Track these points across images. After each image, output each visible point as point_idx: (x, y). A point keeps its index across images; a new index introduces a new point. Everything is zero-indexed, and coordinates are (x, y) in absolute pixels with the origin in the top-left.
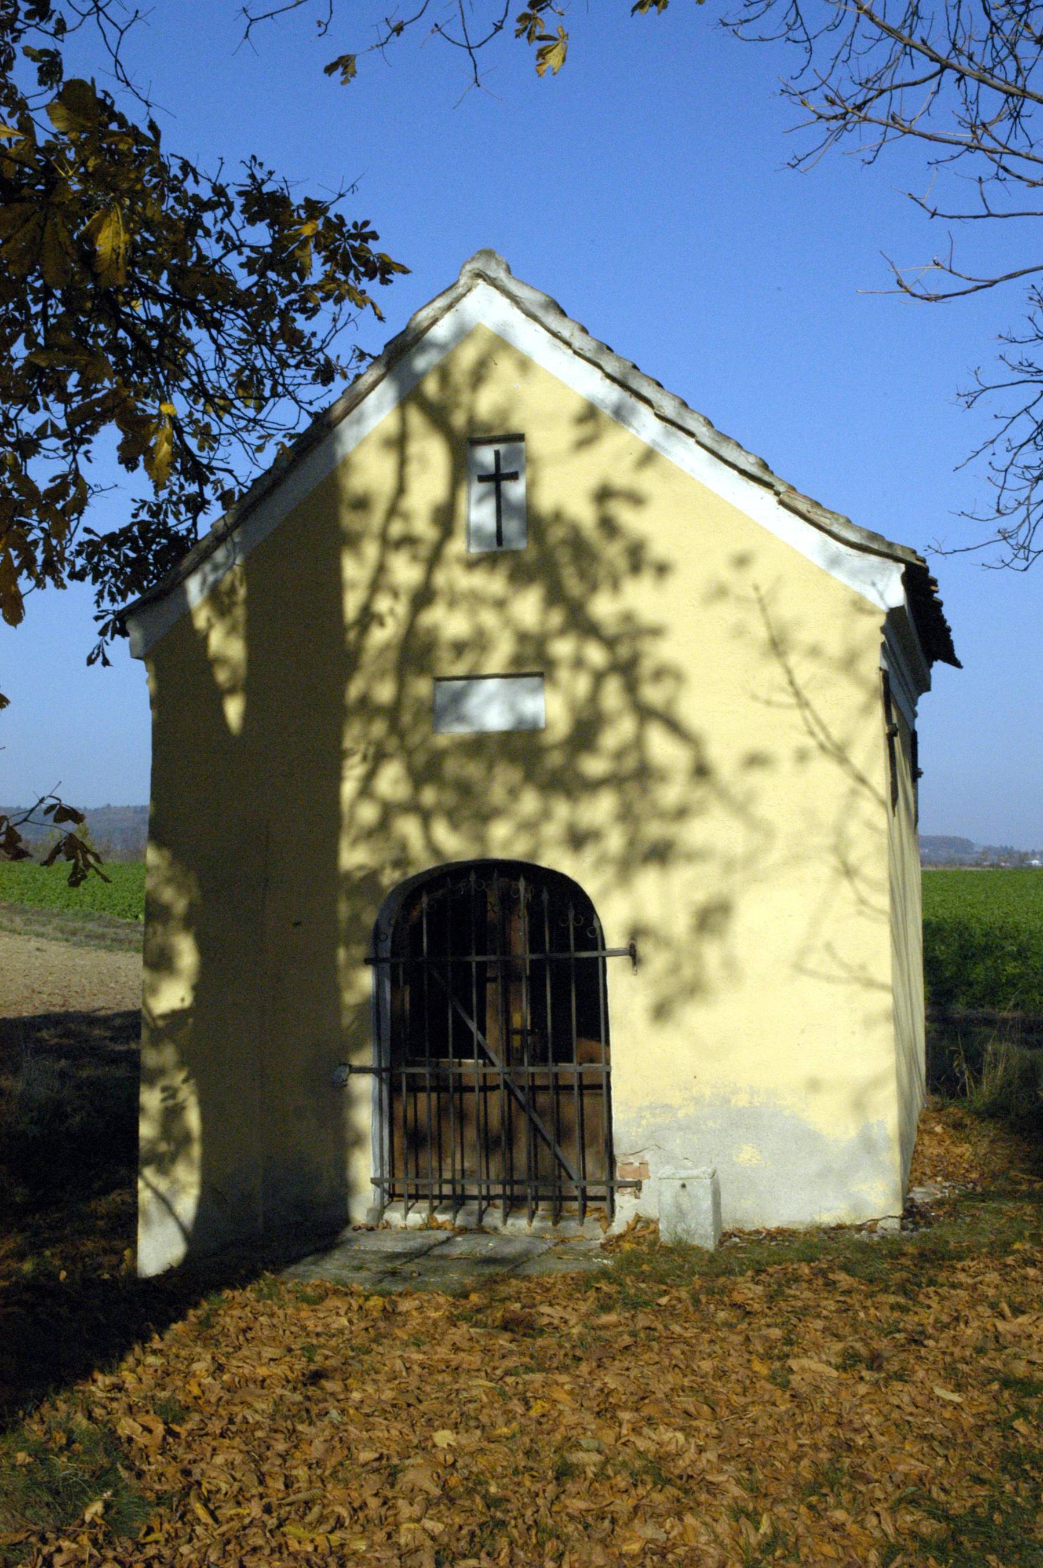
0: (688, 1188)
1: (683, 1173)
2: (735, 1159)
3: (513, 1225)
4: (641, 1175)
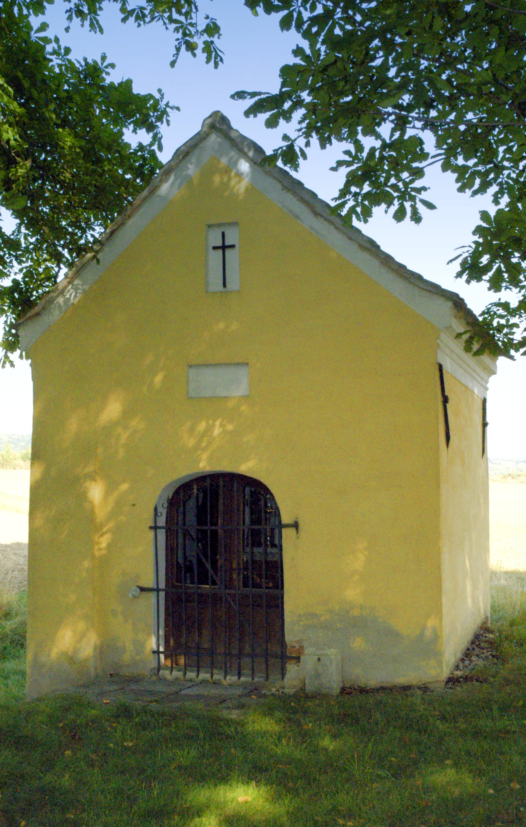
0: (322, 660)
1: (318, 652)
2: (352, 645)
3: (229, 679)
4: (299, 653)
